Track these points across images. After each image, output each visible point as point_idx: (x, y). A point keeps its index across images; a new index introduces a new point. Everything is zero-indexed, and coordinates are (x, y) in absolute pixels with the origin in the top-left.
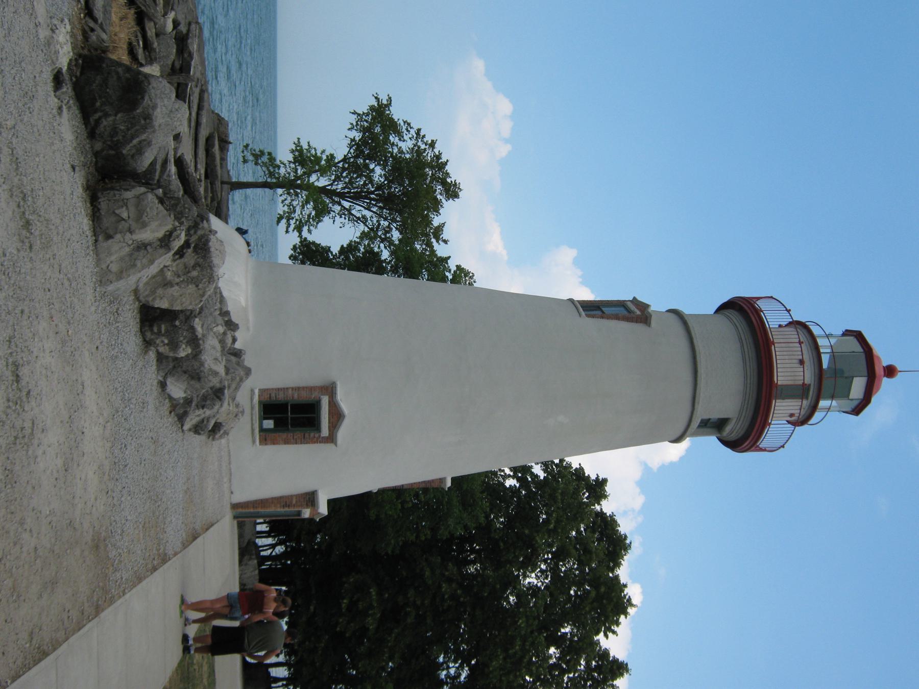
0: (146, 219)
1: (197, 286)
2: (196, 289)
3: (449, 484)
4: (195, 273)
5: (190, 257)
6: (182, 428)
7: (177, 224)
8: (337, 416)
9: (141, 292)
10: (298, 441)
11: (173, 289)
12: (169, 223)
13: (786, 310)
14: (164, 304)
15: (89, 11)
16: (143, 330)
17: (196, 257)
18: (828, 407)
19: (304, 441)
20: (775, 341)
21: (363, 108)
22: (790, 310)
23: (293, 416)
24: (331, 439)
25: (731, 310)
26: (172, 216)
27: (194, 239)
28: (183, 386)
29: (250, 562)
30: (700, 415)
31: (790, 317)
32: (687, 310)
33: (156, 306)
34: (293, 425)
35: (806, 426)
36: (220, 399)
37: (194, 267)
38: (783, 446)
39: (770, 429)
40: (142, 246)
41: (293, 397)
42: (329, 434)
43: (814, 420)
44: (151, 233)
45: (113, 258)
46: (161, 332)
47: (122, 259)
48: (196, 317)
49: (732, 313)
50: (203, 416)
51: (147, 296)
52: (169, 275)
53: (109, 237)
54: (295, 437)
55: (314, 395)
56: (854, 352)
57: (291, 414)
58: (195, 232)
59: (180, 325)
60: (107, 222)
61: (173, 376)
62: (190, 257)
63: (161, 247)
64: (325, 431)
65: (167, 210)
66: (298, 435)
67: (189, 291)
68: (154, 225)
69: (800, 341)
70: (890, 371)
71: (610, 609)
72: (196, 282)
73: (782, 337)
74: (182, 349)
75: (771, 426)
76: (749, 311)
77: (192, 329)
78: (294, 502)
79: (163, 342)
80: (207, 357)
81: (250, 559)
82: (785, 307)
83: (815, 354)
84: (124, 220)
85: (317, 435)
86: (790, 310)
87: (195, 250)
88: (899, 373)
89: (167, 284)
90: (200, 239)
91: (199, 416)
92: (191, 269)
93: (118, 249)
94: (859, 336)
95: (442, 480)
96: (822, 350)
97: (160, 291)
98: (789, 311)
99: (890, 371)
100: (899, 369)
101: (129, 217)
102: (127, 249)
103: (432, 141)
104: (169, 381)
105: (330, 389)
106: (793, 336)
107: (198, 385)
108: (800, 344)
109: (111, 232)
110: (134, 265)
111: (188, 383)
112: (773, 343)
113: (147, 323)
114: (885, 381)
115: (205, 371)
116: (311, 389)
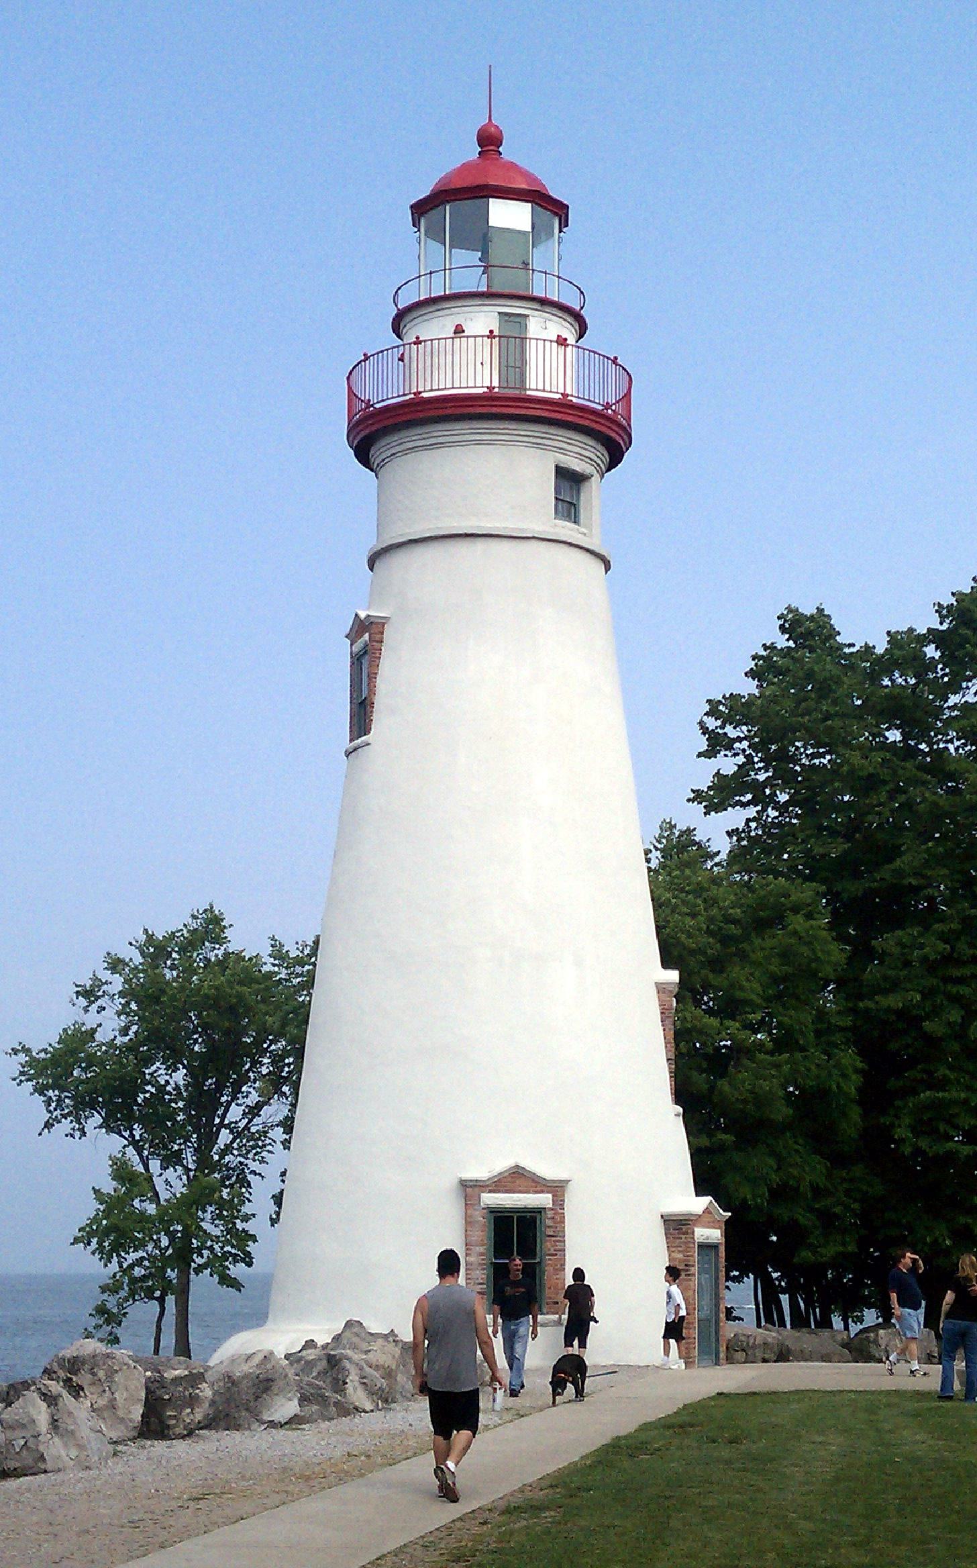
0: (26, 1420)
1: (116, 1371)
2: (120, 1373)
3: (673, 976)
4: (101, 1374)
5: (83, 1378)
6: (367, 1412)
7: (33, 1388)
8: (517, 1178)
9: (120, 1434)
10: (559, 1247)
11: (118, 1398)
12: (32, 1396)
13: (364, 361)
14: (137, 1412)
16: (173, 1437)
17: (83, 1372)
19: (559, 1236)
21: (37, 1109)
24: (558, 1188)
25: (372, 452)
26: (25, 1392)
27: (62, 1374)
28: (279, 1401)
29: (883, 1343)
30: (545, 521)
33: (140, 1419)
36: (341, 1360)
37: (94, 1374)
38: (615, 361)
39: (575, 394)
40: (54, 1423)
41: (482, 1254)
42: (548, 1192)
44: (41, 1413)
45: (63, 1453)
46: (175, 1416)
47: (66, 1445)
48: (163, 1376)
49: (378, 453)
50: (357, 1384)
51: (127, 1427)
52: (102, 1402)
53: (42, 1458)
54: (552, 1252)
55: (479, 1217)
58: (55, 1372)
59: (168, 1394)
60: (28, 1459)
61: (261, 1412)
62: (83, 1378)
63: (56, 1405)
64: (544, 1200)
65: (19, 1397)
66: (549, 1245)
67: (122, 1381)
68: (33, 1413)
69: (415, 343)
70: (489, 140)
71: (287, 1007)
72: (111, 1373)
74: (200, 1394)
75: (569, 391)
77: (177, 1380)
78: (680, 1256)
79: (188, 1414)
81: (876, 1343)
82: (361, 361)
84: (26, 1443)
85: (550, 1214)
86: (616, 358)
87: (75, 1372)
89: (112, 1405)
90: (61, 1367)
91: (355, 1389)
92: (96, 1378)
93: (54, 1449)
94: (420, 209)
95: (661, 988)
97: (121, 1413)
98: (367, 358)
99: (489, 140)
101: (24, 1438)
102: (56, 1439)
104: (266, 1418)
105: (469, 1189)
107: (281, 1383)
109: (37, 1456)
110: (73, 1432)
111: (277, 1394)
113: (166, 1431)
114: (508, 151)
115: (258, 1372)
116: (468, 1222)
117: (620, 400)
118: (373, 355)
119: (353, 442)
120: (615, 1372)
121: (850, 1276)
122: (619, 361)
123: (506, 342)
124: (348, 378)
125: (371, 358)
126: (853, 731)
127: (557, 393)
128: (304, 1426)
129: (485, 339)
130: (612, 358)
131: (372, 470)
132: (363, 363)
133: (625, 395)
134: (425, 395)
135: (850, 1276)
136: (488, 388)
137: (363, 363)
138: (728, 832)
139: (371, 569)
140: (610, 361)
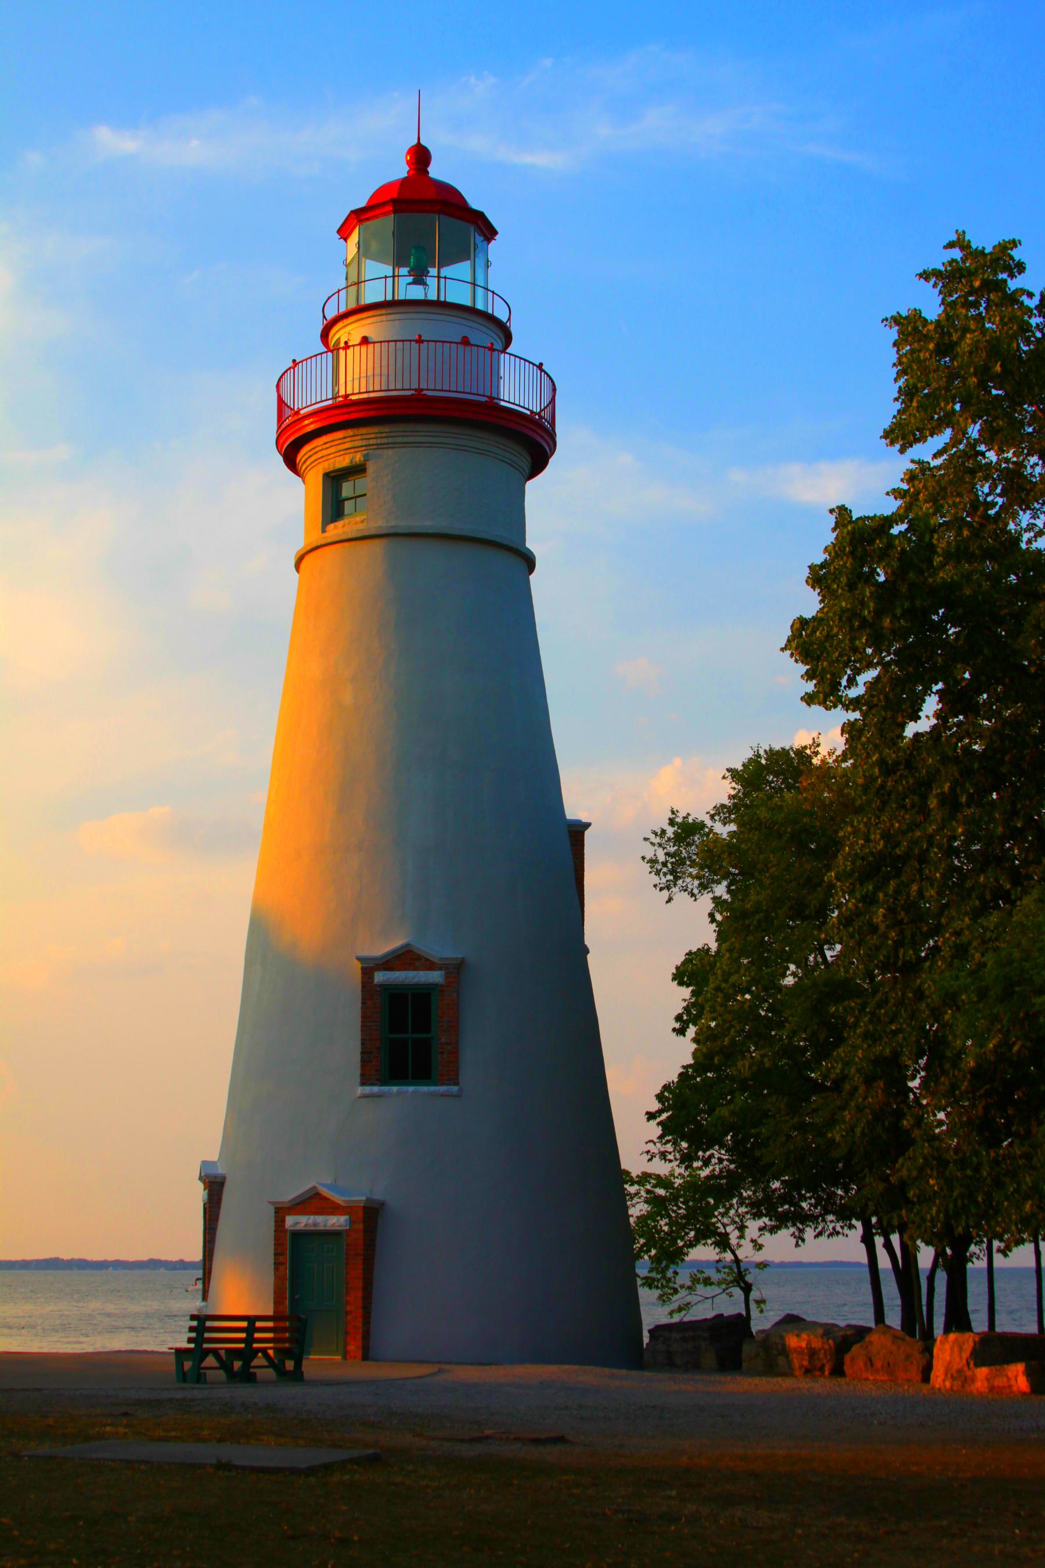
15: (2, 1335)
18: (473, 286)
20: (415, 386)
22: (294, 361)
23: (410, 1031)
31: (314, 359)
32: (299, 544)
34: (427, 1029)
35: (512, 330)
38: (540, 367)
43: (501, 314)
56: (393, 233)
57: (407, 1032)
70: (420, 156)
73: (349, 378)
76: (297, 435)
80: (994, 914)
82: (289, 369)
83: (480, 320)
86: (541, 364)
88: (422, 142)
96: (389, 298)
100: (415, 142)
103: (729, 798)
106: (475, 356)
108: (422, 342)
112: (419, 390)
117: (545, 408)
118: (302, 362)
119: (282, 445)
120: (365, 495)
121: (750, 1180)
122: (544, 367)
123: (433, 347)
124: (278, 386)
125: (300, 364)
126: (747, 981)
127: (484, 396)
128: (262, 1437)
129: (413, 343)
130: (538, 364)
131: (299, 475)
132: (292, 370)
133: (550, 403)
134: (353, 398)
135: (750, 1180)
136: (415, 390)
137: (300, 407)
138: (647, 1113)
139: (298, 573)
140: (535, 368)
